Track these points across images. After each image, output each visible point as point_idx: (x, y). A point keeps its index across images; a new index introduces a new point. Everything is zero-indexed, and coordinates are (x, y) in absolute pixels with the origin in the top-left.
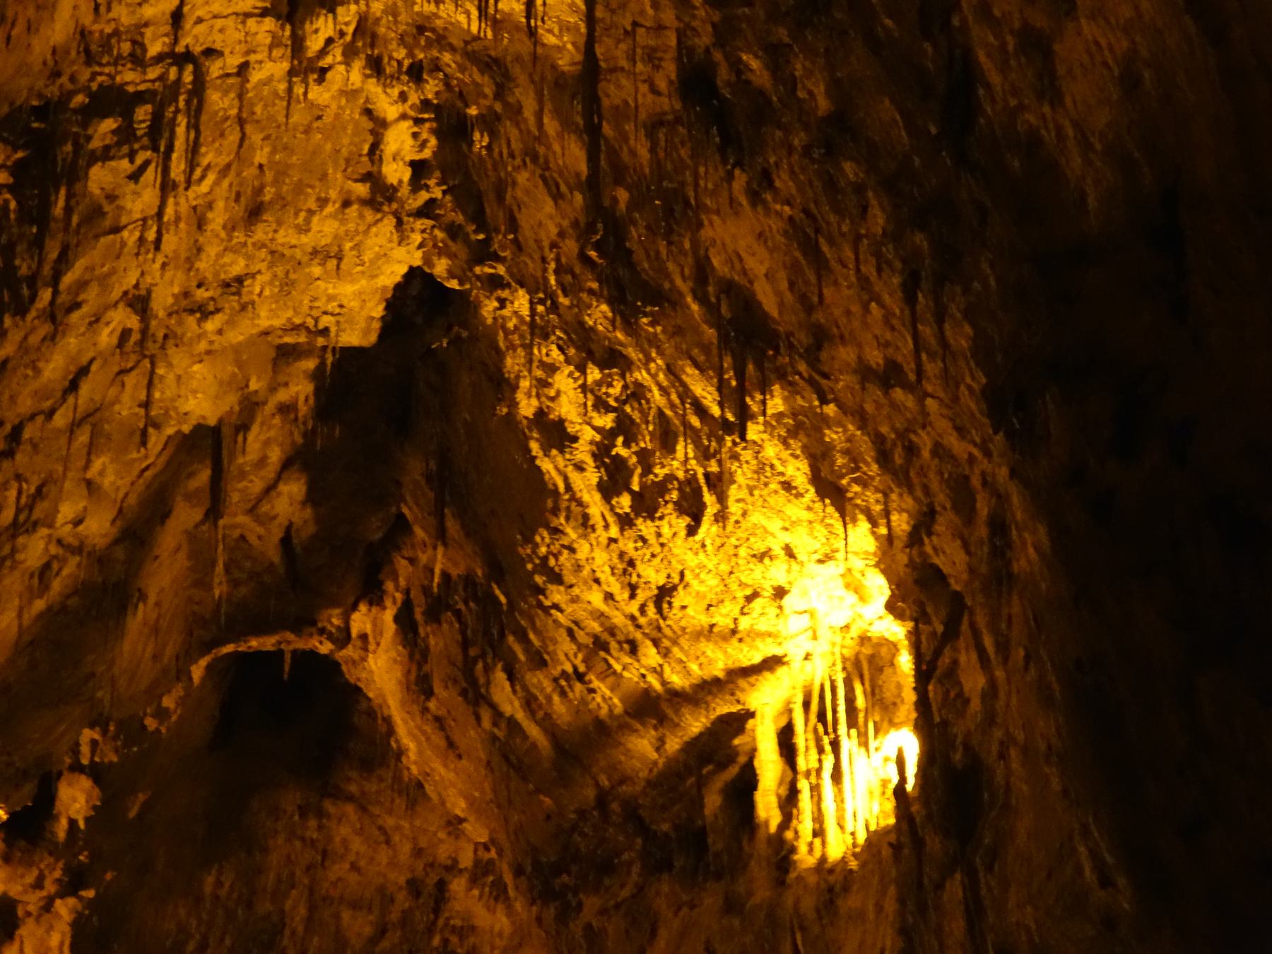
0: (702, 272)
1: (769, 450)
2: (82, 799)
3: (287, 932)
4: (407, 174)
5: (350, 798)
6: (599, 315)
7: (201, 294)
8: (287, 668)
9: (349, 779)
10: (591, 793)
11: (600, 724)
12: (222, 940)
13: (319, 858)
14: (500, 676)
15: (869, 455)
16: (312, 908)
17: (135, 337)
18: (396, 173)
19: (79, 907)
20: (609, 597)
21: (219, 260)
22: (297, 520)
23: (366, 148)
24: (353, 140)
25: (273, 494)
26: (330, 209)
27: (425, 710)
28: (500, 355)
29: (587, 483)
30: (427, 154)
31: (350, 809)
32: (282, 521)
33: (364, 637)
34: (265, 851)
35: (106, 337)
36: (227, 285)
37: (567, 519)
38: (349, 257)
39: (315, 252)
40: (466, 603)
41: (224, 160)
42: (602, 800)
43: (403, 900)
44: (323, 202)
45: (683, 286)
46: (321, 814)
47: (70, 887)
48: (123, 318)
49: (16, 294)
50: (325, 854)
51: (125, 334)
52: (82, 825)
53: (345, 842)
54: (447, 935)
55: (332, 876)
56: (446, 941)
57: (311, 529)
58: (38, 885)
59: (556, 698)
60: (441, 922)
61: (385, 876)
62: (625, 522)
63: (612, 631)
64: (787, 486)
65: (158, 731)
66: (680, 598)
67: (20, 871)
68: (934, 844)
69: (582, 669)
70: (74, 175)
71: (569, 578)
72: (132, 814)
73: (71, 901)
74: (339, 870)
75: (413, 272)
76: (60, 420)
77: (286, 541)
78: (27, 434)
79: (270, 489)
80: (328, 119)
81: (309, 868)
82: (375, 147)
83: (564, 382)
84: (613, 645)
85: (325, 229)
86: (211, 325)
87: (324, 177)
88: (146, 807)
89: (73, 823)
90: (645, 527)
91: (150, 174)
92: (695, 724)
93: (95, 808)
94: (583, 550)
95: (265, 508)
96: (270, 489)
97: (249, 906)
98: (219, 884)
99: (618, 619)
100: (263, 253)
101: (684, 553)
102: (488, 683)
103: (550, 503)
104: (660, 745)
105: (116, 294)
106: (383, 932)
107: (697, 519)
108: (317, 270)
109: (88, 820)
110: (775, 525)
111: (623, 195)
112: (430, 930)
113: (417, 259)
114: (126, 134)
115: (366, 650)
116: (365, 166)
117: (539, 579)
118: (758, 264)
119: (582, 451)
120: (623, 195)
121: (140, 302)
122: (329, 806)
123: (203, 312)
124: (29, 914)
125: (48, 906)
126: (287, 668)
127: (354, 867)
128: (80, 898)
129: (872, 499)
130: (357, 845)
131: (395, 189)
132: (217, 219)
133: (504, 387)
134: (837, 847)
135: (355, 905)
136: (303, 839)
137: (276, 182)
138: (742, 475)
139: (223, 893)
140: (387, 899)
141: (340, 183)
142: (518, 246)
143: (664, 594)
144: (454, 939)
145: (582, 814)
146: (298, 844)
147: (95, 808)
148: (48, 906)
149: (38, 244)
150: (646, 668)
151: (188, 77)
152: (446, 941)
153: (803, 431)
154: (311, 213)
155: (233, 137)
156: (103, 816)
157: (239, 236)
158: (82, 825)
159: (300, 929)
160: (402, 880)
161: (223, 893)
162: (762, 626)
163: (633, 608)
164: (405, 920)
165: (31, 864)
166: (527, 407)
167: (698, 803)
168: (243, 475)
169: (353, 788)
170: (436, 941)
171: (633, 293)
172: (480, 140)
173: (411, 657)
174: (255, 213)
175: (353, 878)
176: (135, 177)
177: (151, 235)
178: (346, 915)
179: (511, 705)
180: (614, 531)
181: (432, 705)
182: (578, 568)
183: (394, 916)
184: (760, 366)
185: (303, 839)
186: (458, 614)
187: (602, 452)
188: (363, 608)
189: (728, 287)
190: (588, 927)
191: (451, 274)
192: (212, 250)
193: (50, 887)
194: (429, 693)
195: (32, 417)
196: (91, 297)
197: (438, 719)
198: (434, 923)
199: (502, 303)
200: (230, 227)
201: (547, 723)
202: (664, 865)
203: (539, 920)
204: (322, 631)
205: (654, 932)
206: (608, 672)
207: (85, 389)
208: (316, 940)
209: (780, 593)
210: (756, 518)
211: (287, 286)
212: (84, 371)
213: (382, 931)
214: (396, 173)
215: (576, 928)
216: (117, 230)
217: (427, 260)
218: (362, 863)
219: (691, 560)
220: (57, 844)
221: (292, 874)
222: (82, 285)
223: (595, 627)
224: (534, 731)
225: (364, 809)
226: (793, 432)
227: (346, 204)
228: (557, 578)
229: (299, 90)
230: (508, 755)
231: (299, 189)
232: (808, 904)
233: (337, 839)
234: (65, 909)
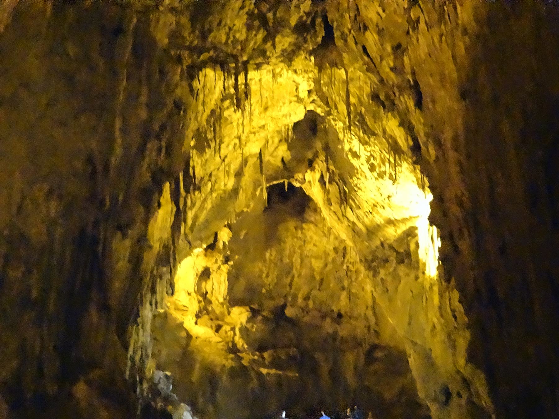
0: (384, 132)
2: (226, 235)
3: (294, 268)
5: (311, 222)
8: (286, 187)
9: (310, 216)
10: (378, 243)
11: (378, 225)
12: (274, 273)
13: (303, 243)
14: (349, 210)
16: (302, 260)
17: (238, 144)
19: (229, 268)
21: (257, 122)
22: (285, 156)
23: (295, 90)
25: (277, 150)
26: (286, 105)
27: (330, 209)
29: (366, 168)
30: (312, 88)
31: (312, 226)
33: (310, 182)
34: (285, 242)
35: (231, 147)
36: (260, 127)
37: (361, 175)
38: (292, 113)
39: (283, 115)
40: (339, 180)
42: (382, 244)
43: (332, 254)
44: (284, 104)
46: (302, 229)
47: (227, 260)
50: (304, 242)
51: (235, 145)
52: (227, 243)
53: (311, 238)
54: (348, 264)
55: (308, 249)
56: (348, 267)
57: (290, 157)
58: (216, 262)
59: (365, 217)
60: (346, 260)
61: (325, 247)
65: (247, 211)
67: (210, 258)
69: (371, 211)
72: (242, 237)
73: (226, 266)
74: (309, 247)
77: (283, 160)
78: (213, 174)
79: (277, 148)
81: (300, 247)
82: (297, 89)
84: (378, 206)
87: (284, 97)
88: (246, 234)
89: (224, 243)
92: (403, 228)
93: (231, 238)
95: (275, 154)
96: (277, 148)
97: (281, 260)
98: (271, 255)
100: (269, 118)
102: (345, 212)
103: (356, 171)
104: (396, 231)
105: (233, 137)
106: (326, 265)
109: (229, 242)
111: (363, 109)
112: (342, 263)
115: (311, 186)
117: (356, 188)
119: (363, 159)
120: (363, 109)
121: (239, 138)
122: (304, 226)
124: (214, 271)
125: (219, 268)
126: (286, 187)
127: (315, 245)
128: (228, 265)
130: (315, 238)
131: (303, 99)
135: (317, 258)
136: (297, 238)
139: (272, 258)
140: (327, 254)
141: (288, 98)
142: (338, 112)
144: (351, 266)
145: (377, 247)
146: (295, 240)
147: (231, 238)
148: (219, 268)
150: (388, 214)
152: (348, 267)
154: (281, 107)
156: (234, 239)
157: (263, 115)
158: (227, 243)
159: (298, 267)
160: (331, 248)
161: (272, 258)
164: (334, 261)
165: (213, 257)
166: (347, 147)
167: (408, 245)
169: (312, 219)
170: (345, 267)
173: (324, 193)
174: (266, 109)
175: (315, 249)
177: (241, 121)
178: (313, 261)
179: (352, 218)
181: (332, 208)
183: (330, 259)
185: (297, 238)
186: (337, 184)
187: (368, 160)
188: (309, 171)
189: (391, 137)
190: (382, 279)
193: (219, 263)
194: (330, 204)
195: (214, 170)
197: (334, 212)
198: (344, 261)
200: (260, 114)
201: (363, 223)
202: (402, 262)
203: (368, 276)
204: (296, 180)
205: (400, 282)
206: (378, 213)
208: (304, 270)
213: (326, 265)
214: (303, 94)
215: (378, 279)
218: (317, 244)
220: (220, 250)
221: (295, 249)
224: (360, 225)
225: (316, 226)
227: (290, 102)
230: (353, 228)
231: (278, 101)
233: (308, 237)
234: (225, 268)
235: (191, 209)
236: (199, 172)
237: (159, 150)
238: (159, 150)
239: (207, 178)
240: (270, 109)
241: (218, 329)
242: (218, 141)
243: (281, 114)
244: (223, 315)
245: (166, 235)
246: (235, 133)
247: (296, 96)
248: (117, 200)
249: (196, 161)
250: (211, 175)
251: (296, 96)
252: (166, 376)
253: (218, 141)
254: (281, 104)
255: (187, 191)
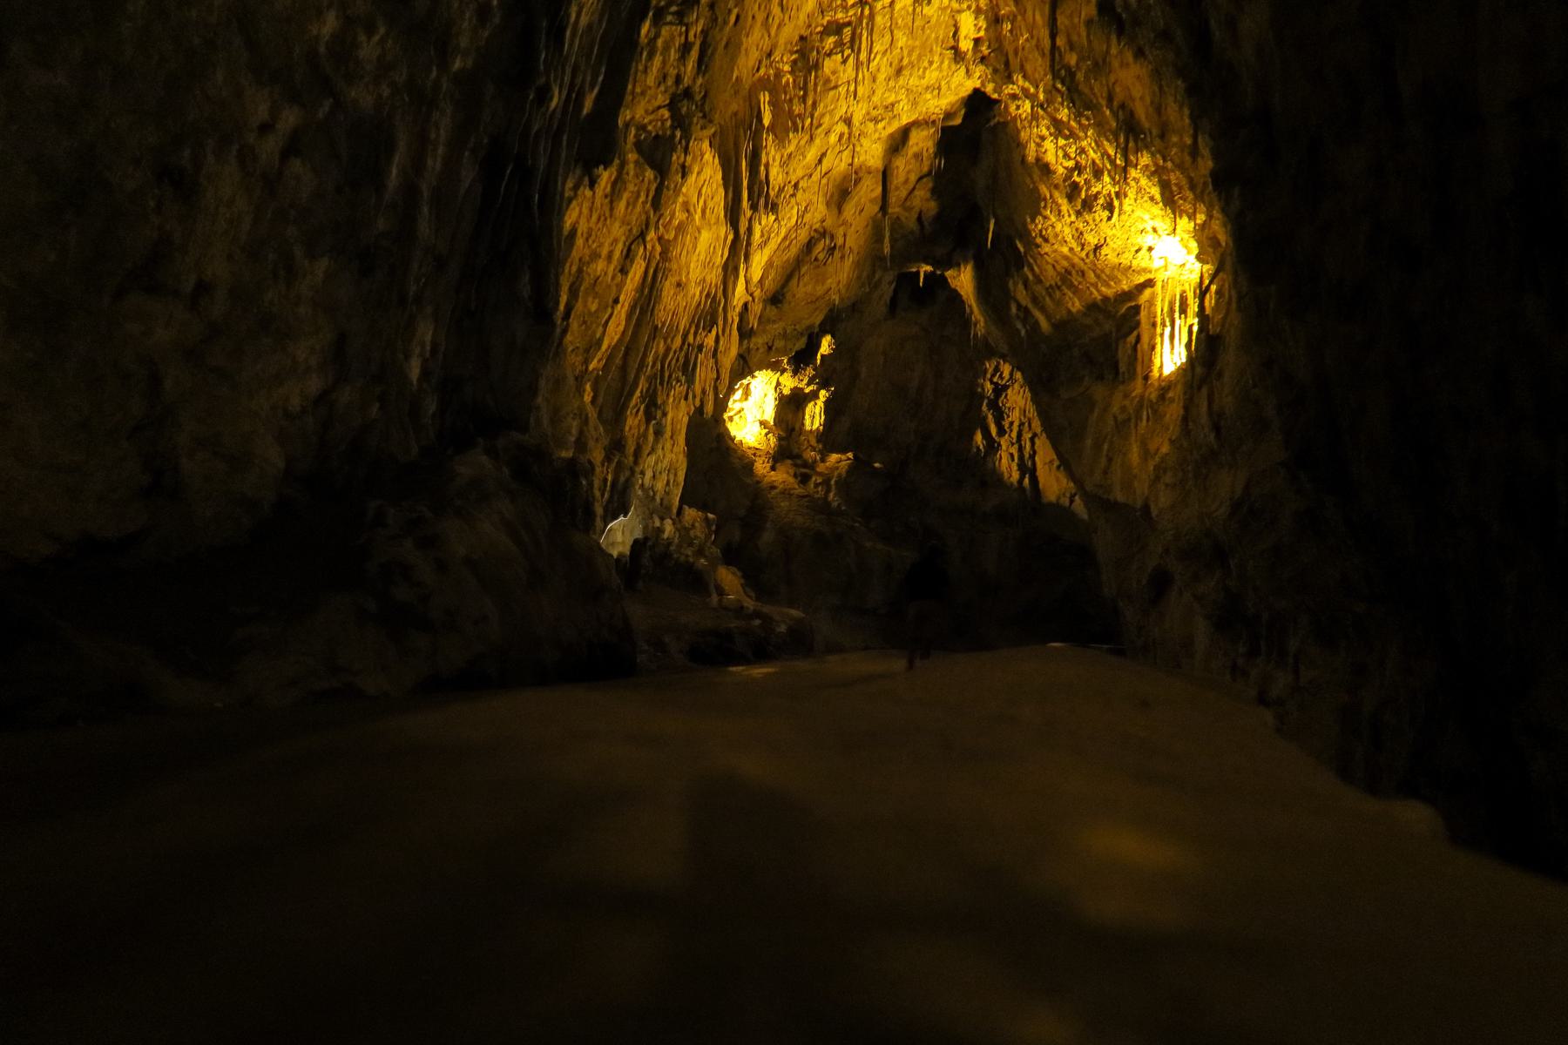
1: (1142, 182)
4: (971, 45)
6: (1064, 114)
7: (874, 113)
15: (1186, 187)
18: (966, 45)
20: (1071, 249)
21: (882, 95)
24: (944, 32)
28: (1018, 132)
30: (982, 33)
32: (917, 210)
35: (833, 138)
38: (944, 87)
41: (883, 49)
45: (1104, 102)
48: (841, 128)
49: (795, 123)
51: (842, 135)
62: (1079, 214)
63: (1073, 266)
64: (1152, 199)
66: (1104, 251)
68: (1199, 370)
70: (817, 66)
71: (1052, 240)
75: (976, 91)
76: (815, 177)
77: (919, 219)
80: (933, 20)
83: (1049, 145)
85: (932, 76)
86: (880, 125)
90: (1088, 217)
91: (851, 60)
94: (1059, 227)
99: (1076, 260)
101: (1105, 229)
107: (1112, 213)
108: (929, 96)
110: (1146, 216)
113: (978, 84)
114: (840, 44)
116: (952, 43)
118: (1137, 92)
121: (848, 121)
123: (876, 120)
129: (1188, 207)
132: (881, 77)
133: (1021, 146)
134: (1167, 371)
137: (910, 55)
138: (1131, 194)
143: (1097, 248)
149: (804, 99)
151: (867, 12)
153: (1157, 173)
155: (888, 37)
162: (1144, 264)
163: (1083, 254)
168: (897, 188)
171: (1080, 102)
172: (1007, 26)
174: (899, 71)
176: (844, 62)
177: (852, 88)
180: (1073, 218)
182: (1056, 235)
184: (1136, 141)
191: (995, 91)
192: (879, 92)
196: (826, 120)
199: (1018, 107)
207: (825, 162)
209: (1150, 249)
210: (1138, 213)
211: (915, 103)
212: (824, 155)
214: (966, 45)
216: (836, 87)
217: (983, 84)
219: (1110, 233)
222: (823, 115)
223: (1065, 264)
226: (1153, 173)
228: (1046, 240)
229: (918, 10)
231: (920, 57)
232: (1154, 397)
235: (762, 246)
236: (776, 176)
237: (686, 48)
238: (686, 48)
239: (789, 190)
240: (906, 72)
241: (804, 479)
242: (810, 102)
243: (924, 82)
244: (815, 461)
245: (714, 277)
246: (841, 111)
247: (952, 48)
248: (579, 104)
249: (772, 154)
250: (796, 186)
251: (952, 48)
252: (707, 519)
253: (810, 102)
254: (926, 64)
255: (754, 207)
